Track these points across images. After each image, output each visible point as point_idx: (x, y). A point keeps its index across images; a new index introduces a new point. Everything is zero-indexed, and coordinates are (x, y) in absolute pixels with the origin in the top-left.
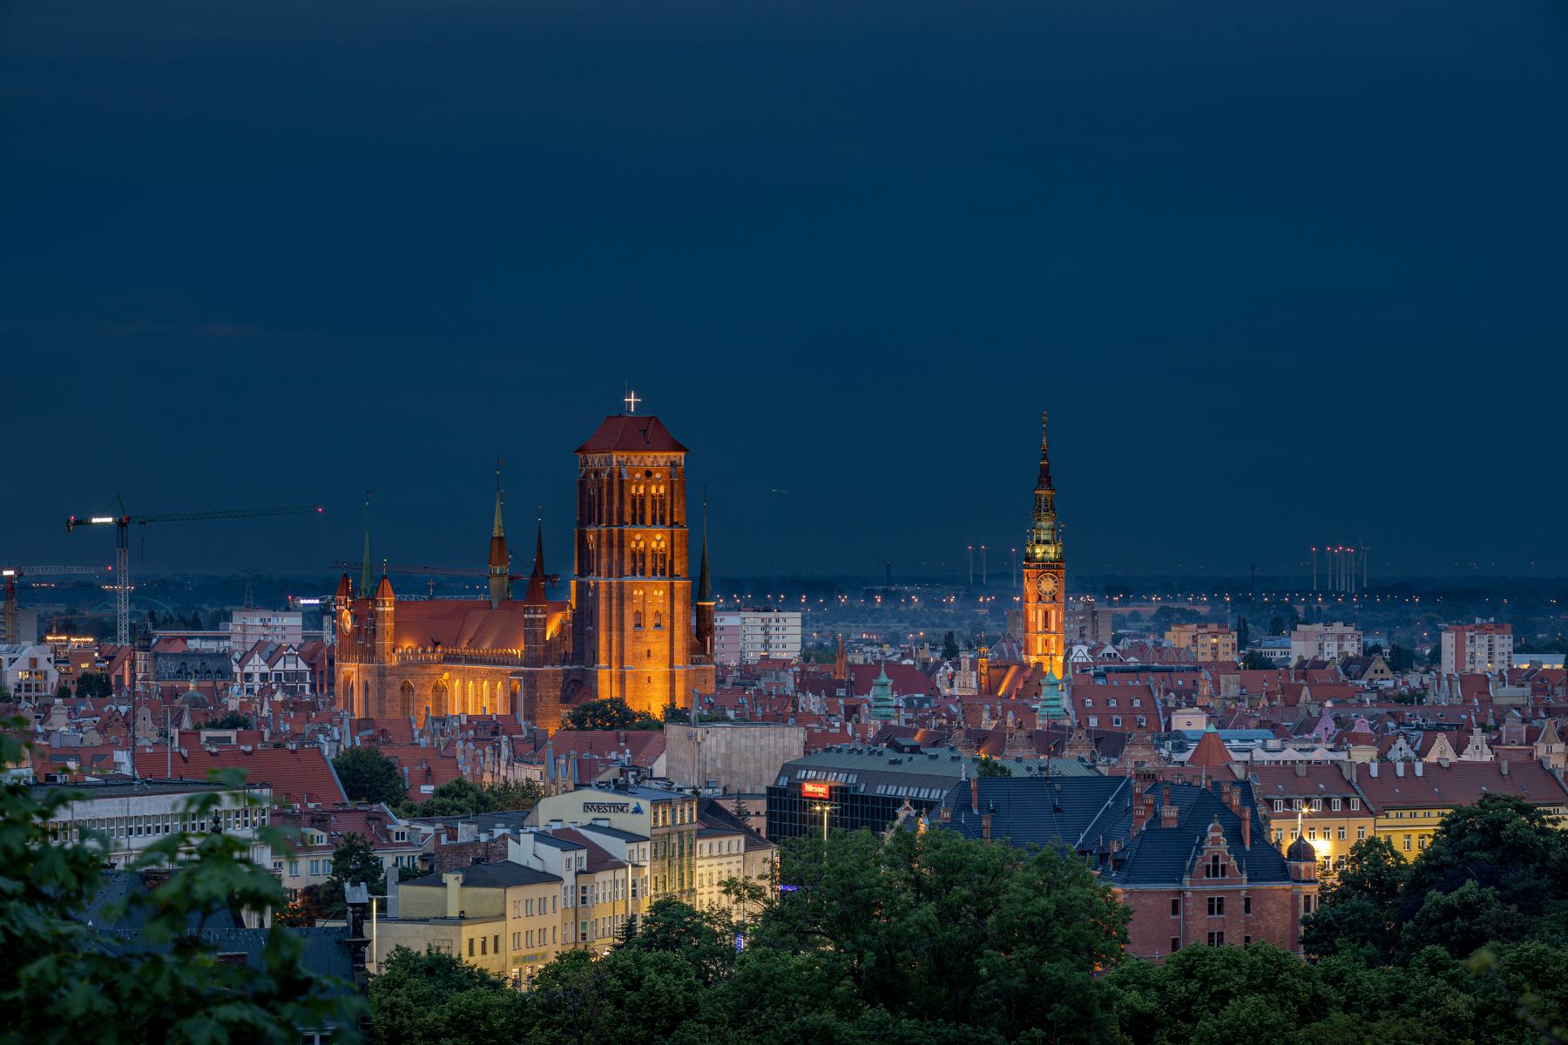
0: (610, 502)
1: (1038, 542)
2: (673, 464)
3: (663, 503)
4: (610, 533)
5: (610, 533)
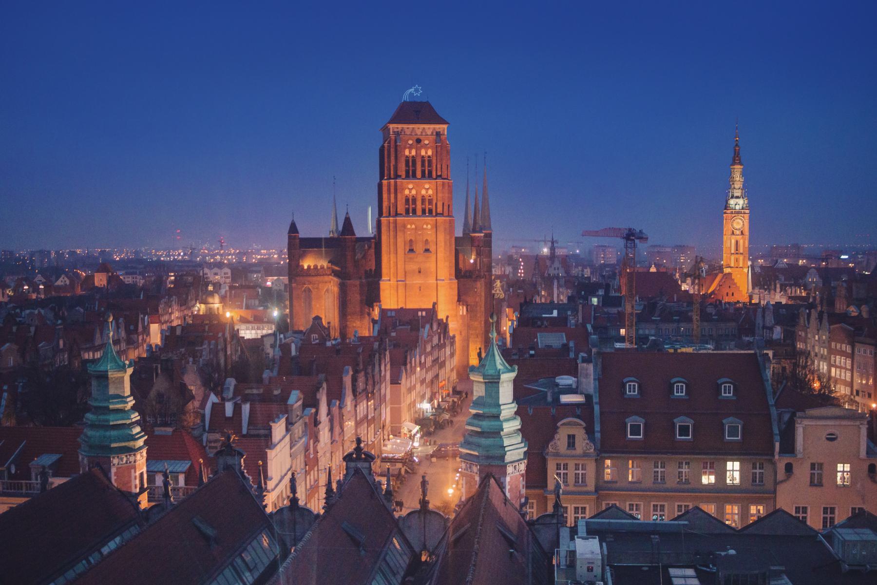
0: (389, 162)
1: (732, 197)
2: (438, 134)
3: (430, 162)
4: (389, 185)
5: (389, 185)
